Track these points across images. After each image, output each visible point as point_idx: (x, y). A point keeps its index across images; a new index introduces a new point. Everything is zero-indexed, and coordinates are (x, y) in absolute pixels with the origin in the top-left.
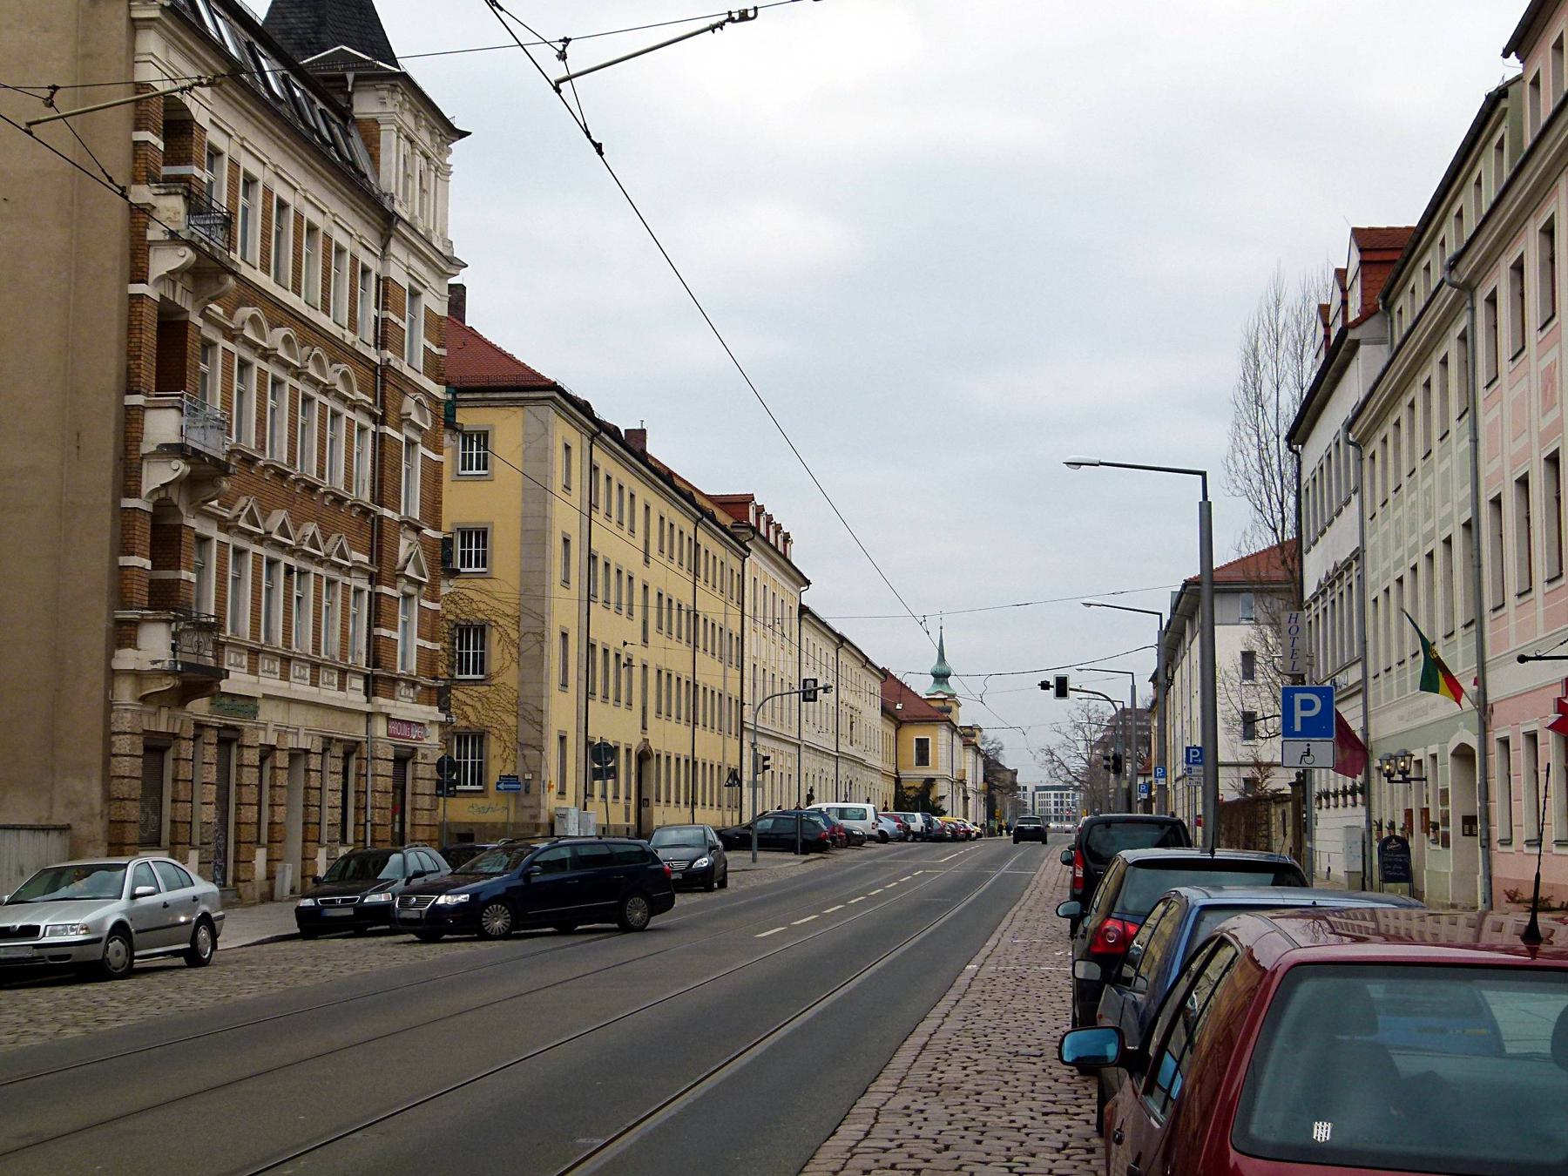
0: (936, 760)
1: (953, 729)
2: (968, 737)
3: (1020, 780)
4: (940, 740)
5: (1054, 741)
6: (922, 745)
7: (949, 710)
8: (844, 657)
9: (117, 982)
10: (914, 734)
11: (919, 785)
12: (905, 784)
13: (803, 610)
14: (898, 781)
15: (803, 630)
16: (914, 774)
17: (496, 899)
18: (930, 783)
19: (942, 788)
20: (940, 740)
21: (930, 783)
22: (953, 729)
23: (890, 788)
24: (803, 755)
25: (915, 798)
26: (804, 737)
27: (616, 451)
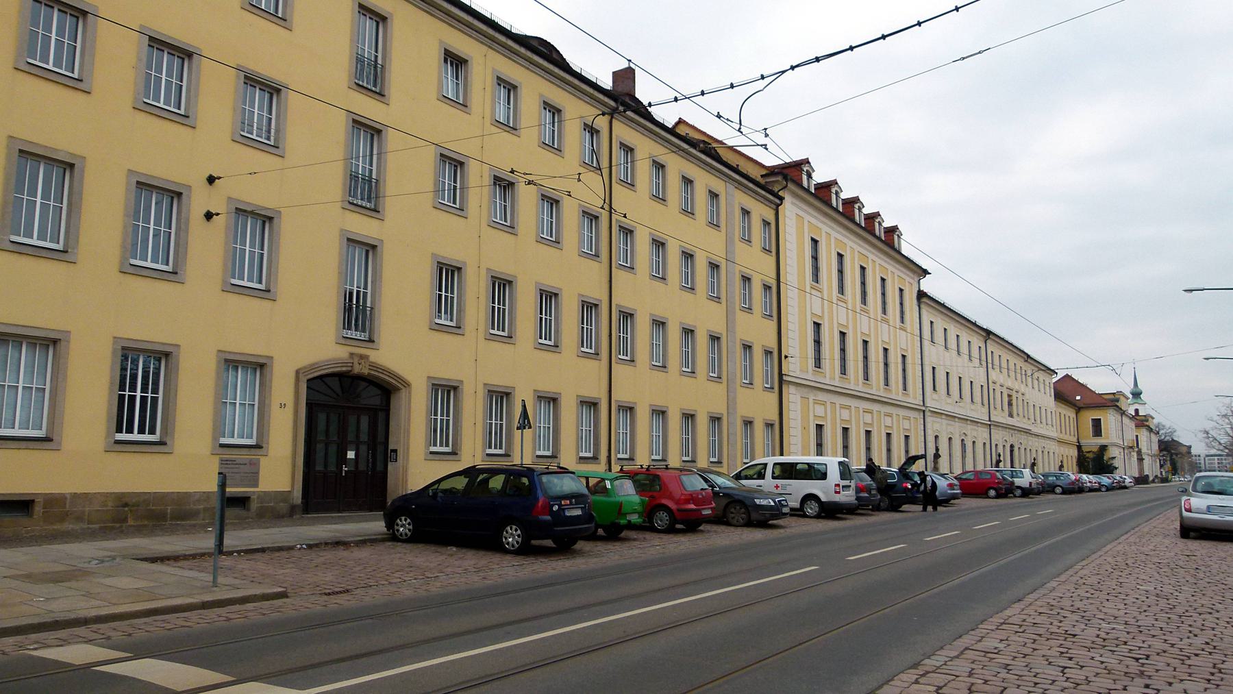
0: (1107, 429)
1: (1150, 430)
2: (1141, 422)
3: (1193, 451)
4: (1110, 420)
5: (1209, 425)
6: (1097, 424)
7: (1118, 400)
8: (991, 346)
9: (599, 543)
10: (1089, 416)
11: (1095, 450)
12: (1085, 449)
13: (921, 295)
14: (1079, 447)
15: (924, 312)
16: (1092, 443)
17: (507, 552)
18: (1103, 448)
19: (1113, 452)
20: (1110, 420)
21: (1103, 448)
22: (1150, 430)
23: (1075, 453)
24: (928, 419)
25: (1096, 462)
26: (928, 403)
27: (763, 197)
